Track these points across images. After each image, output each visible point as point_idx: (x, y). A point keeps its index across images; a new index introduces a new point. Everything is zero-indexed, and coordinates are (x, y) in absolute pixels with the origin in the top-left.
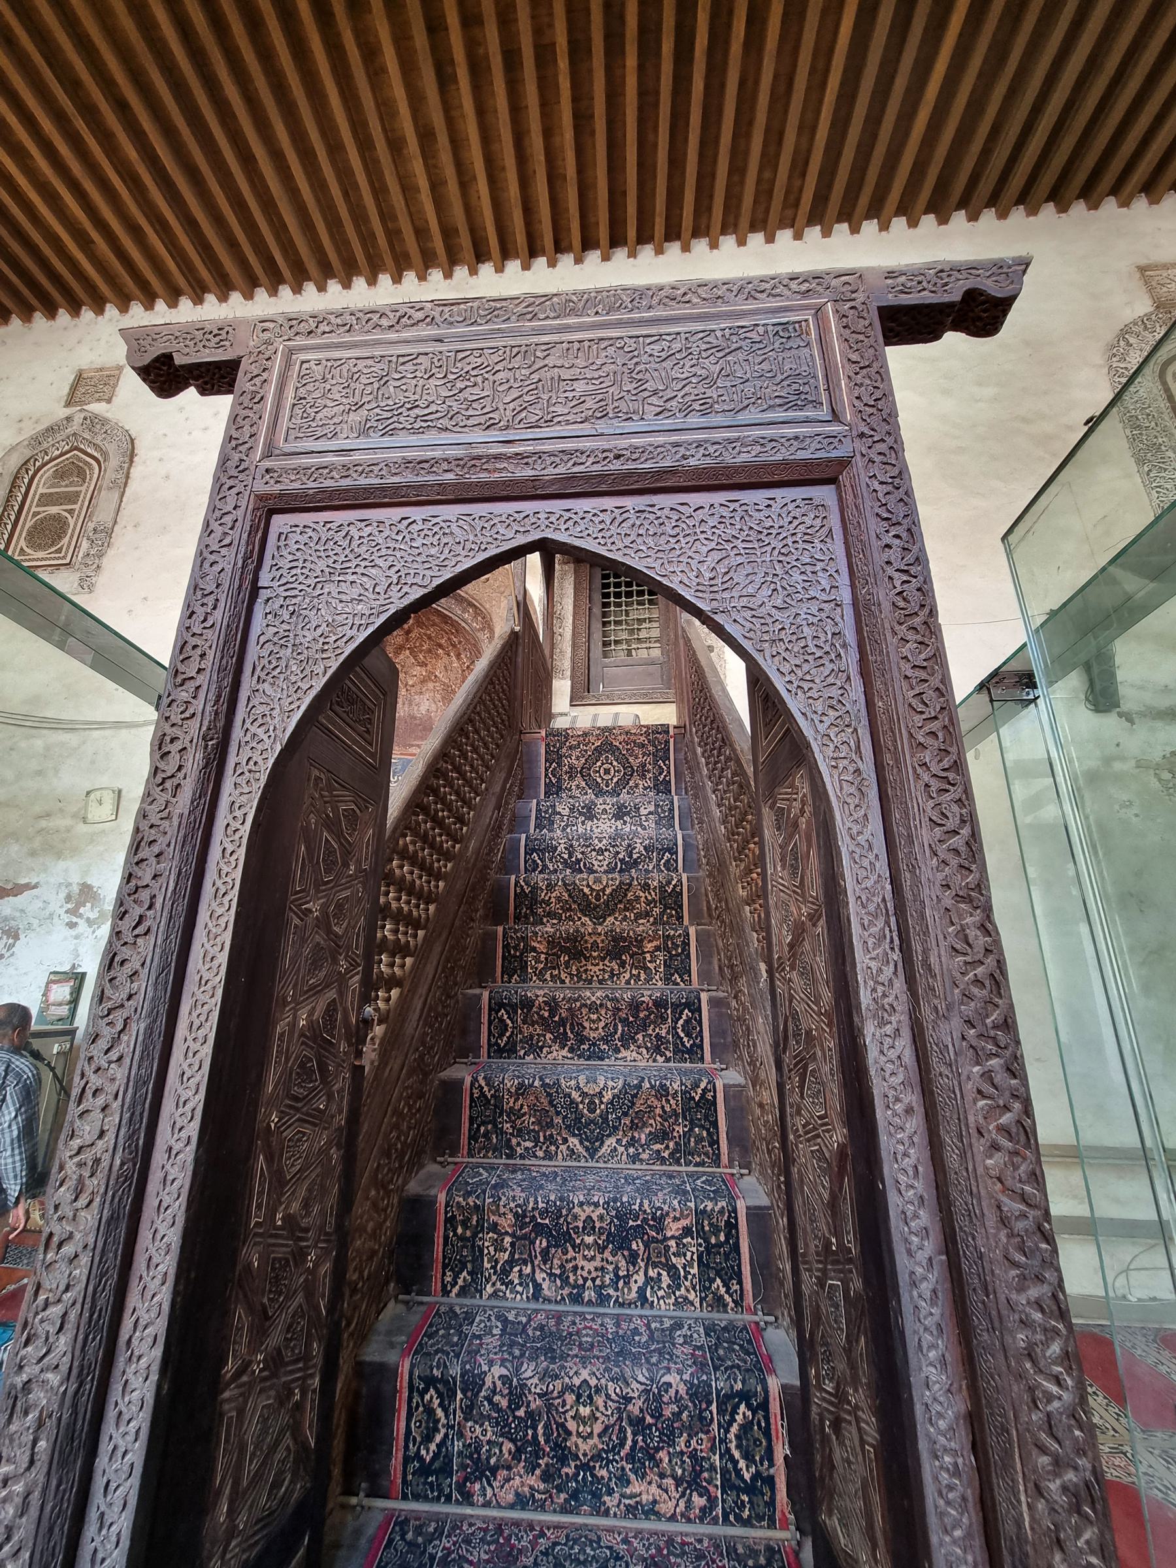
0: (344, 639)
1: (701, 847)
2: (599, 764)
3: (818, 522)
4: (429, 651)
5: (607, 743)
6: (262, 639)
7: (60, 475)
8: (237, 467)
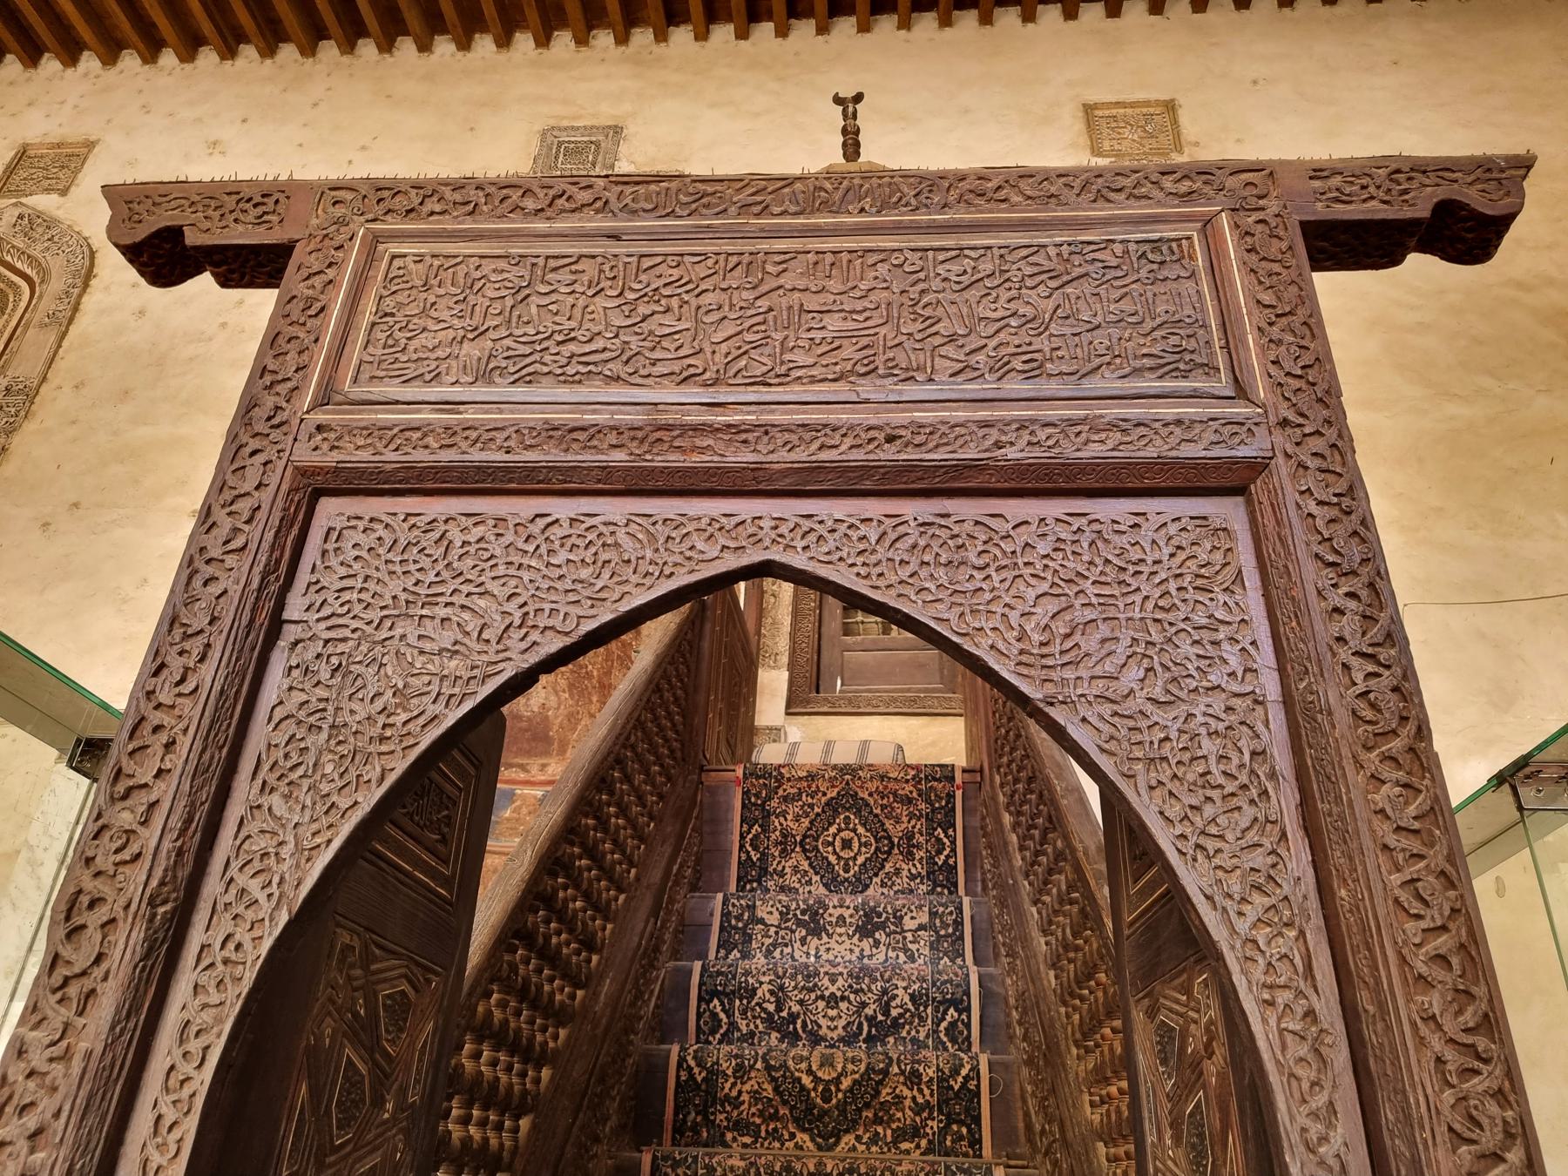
0: (421, 721)
1: (1012, 1001)
2: (833, 830)
3: (1218, 557)
5: (847, 792)
6: (279, 713)
8: (269, 419)
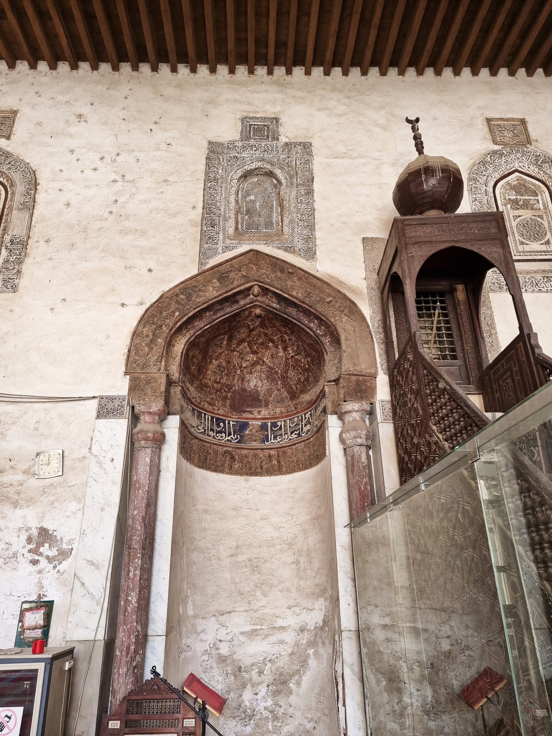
4: (262, 344)
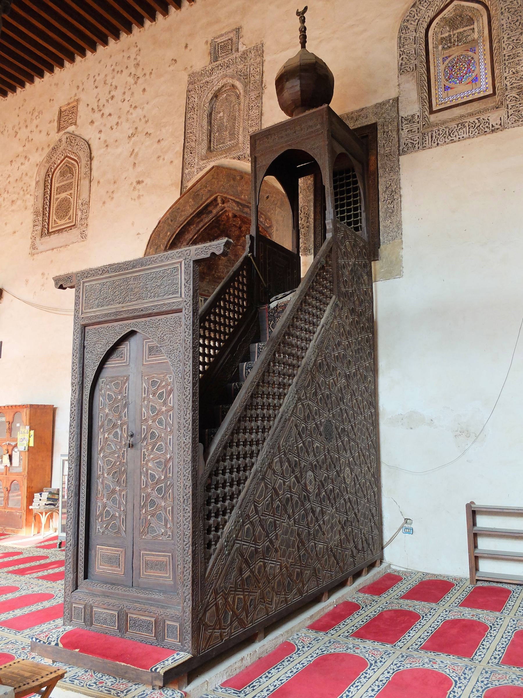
7: (63, 174)
